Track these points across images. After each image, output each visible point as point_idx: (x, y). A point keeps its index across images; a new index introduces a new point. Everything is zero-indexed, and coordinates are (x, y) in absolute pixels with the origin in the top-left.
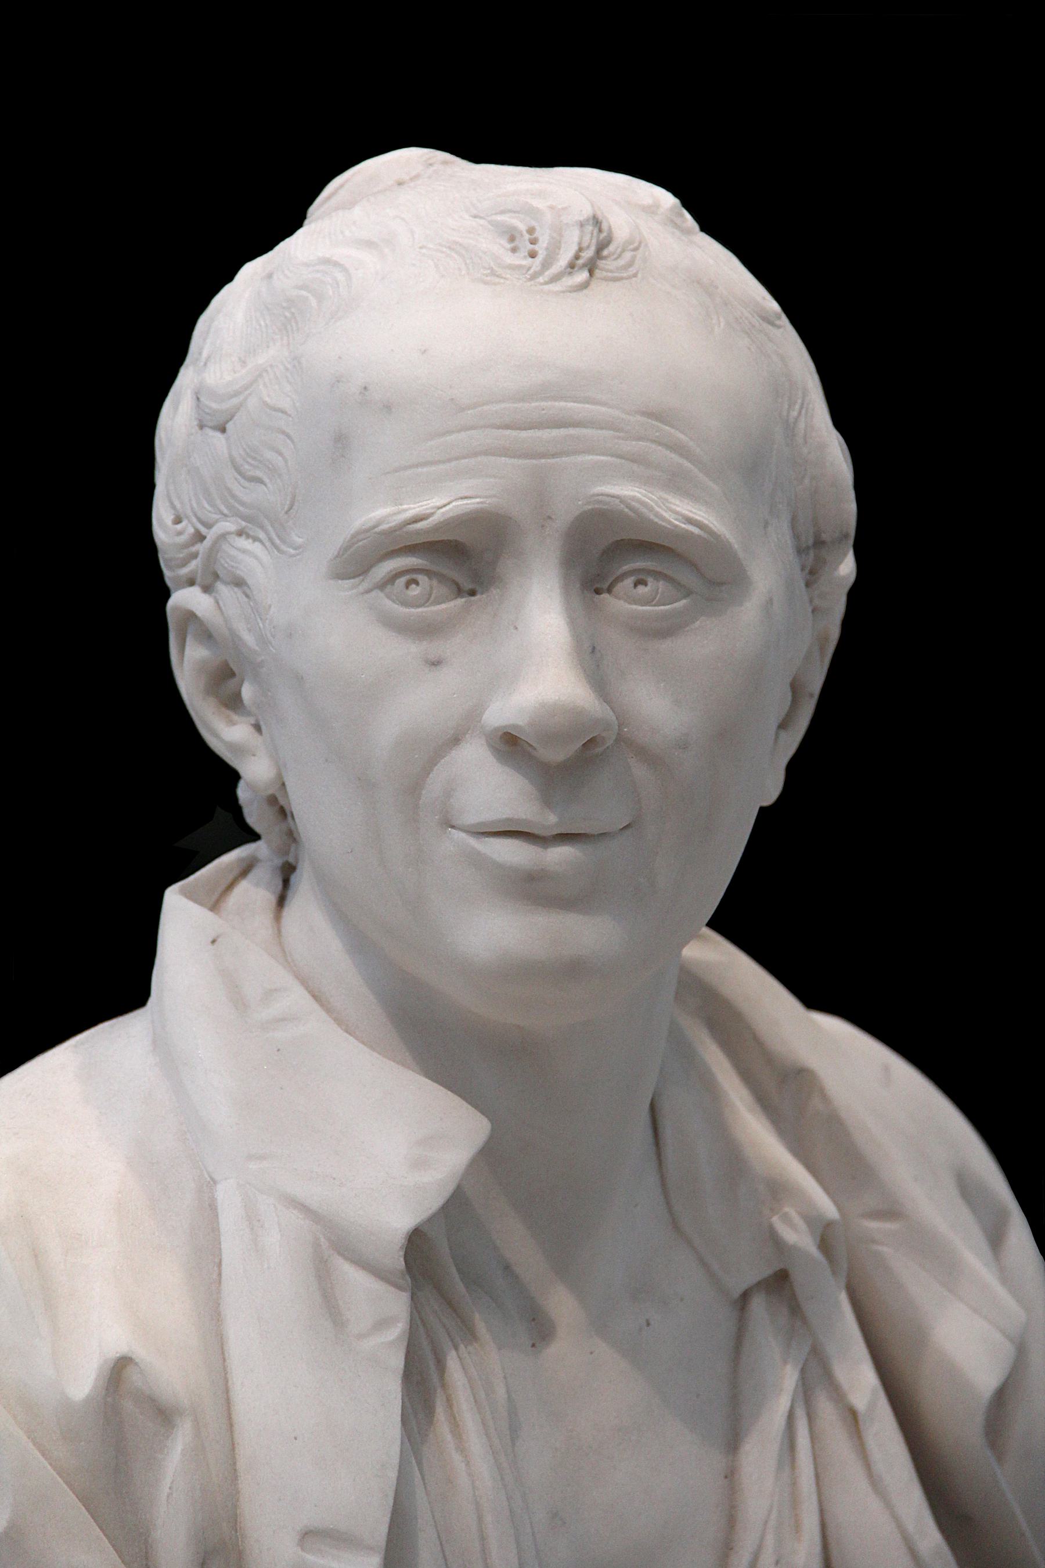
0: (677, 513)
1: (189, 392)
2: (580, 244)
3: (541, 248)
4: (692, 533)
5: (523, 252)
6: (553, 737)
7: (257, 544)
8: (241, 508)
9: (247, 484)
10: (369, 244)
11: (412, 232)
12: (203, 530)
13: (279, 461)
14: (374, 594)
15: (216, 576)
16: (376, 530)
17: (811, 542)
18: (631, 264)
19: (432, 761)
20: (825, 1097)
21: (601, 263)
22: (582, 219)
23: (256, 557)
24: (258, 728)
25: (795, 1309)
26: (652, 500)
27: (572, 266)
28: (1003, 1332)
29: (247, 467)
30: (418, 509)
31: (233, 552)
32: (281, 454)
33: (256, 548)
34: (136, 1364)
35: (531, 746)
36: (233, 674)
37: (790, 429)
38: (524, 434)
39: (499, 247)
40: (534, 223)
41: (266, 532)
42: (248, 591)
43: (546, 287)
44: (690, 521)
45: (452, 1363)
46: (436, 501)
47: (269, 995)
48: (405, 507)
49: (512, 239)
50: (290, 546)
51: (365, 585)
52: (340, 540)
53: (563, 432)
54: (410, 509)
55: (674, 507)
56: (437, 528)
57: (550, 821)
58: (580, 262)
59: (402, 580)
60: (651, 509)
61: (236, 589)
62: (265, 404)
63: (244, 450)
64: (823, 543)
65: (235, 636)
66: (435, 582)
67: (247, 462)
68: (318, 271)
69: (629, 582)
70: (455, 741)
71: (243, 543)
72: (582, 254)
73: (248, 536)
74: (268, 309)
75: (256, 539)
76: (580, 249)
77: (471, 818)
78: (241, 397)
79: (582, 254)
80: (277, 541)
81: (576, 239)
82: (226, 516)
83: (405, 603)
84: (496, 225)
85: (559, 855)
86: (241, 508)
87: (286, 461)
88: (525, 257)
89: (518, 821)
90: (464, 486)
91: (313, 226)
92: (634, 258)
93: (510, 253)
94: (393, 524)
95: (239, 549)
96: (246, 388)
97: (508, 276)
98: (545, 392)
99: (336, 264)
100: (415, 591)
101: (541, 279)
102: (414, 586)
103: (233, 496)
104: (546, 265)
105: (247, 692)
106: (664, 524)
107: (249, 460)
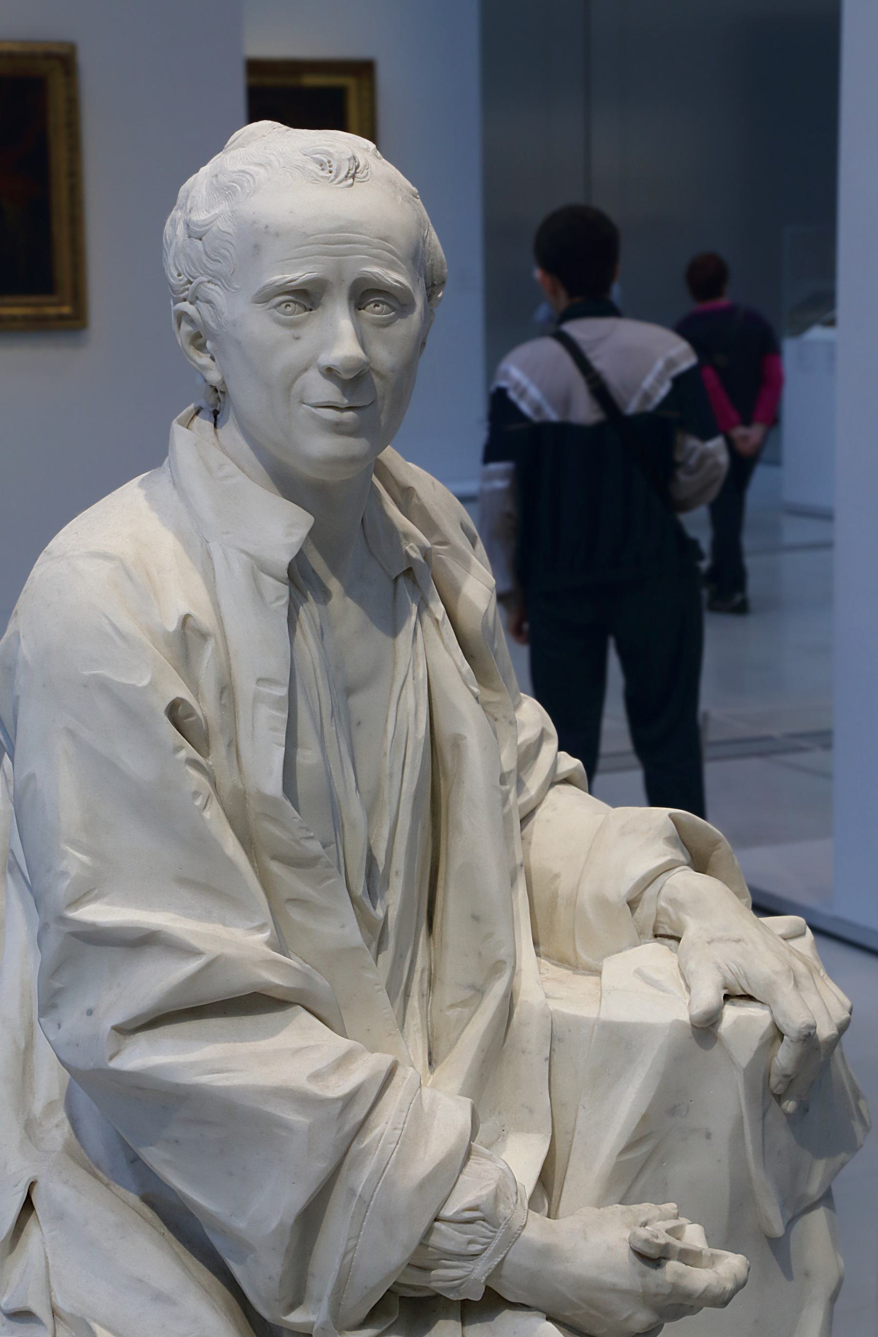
0: (392, 278)
1: (182, 223)
2: (349, 168)
3: (334, 169)
4: (398, 286)
7: (217, 286)
8: (210, 272)
9: (213, 262)
10: (260, 165)
11: (279, 161)
12: (191, 279)
13: (227, 253)
14: (272, 310)
15: (197, 298)
16: (274, 285)
18: (367, 175)
20: (419, 499)
22: (349, 157)
23: (217, 292)
24: (213, 359)
25: (415, 582)
26: (383, 273)
28: (489, 589)
29: (212, 255)
30: (292, 277)
31: (206, 289)
32: (228, 251)
33: (217, 288)
34: (192, 617)
35: (338, 372)
36: (201, 337)
38: (333, 247)
39: (315, 168)
40: (330, 159)
41: (222, 282)
42: (213, 306)
43: (337, 186)
44: (397, 281)
45: (301, 609)
46: (299, 274)
47: (221, 466)
48: (286, 276)
49: (321, 165)
50: (233, 288)
51: (268, 306)
52: (257, 289)
53: (348, 246)
54: (288, 277)
55: (391, 276)
56: (300, 284)
58: (350, 175)
59: (284, 305)
60: (383, 277)
61: (207, 304)
62: (221, 230)
63: (212, 248)
64: (435, 285)
65: (205, 323)
66: (297, 306)
67: (213, 254)
68: (239, 176)
69: (372, 305)
71: (210, 286)
72: (350, 172)
73: (212, 283)
74: (218, 190)
75: (216, 284)
76: (349, 170)
78: (209, 227)
79: (350, 172)
80: (227, 286)
81: (348, 166)
82: (203, 274)
83: (284, 314)
84: (314, 159)
85: (349, 415)
86: (210, 272)
87: (231, 255)
88: (328, 173)
90: (310, 268)
91: (233, 153)
92: (368, 172)
93: (321, 171)
94: (281, 283)
95: (209, 289)
96: (211, 223)
97: (322, 181)
98: (341, 229)
99: (247, 173)
100: (289, 309)
101: (335, 182)
102: (288, 307)
103: (207, 268)
105: (209, 344)
106: (388, 283)
107: (213, 252)
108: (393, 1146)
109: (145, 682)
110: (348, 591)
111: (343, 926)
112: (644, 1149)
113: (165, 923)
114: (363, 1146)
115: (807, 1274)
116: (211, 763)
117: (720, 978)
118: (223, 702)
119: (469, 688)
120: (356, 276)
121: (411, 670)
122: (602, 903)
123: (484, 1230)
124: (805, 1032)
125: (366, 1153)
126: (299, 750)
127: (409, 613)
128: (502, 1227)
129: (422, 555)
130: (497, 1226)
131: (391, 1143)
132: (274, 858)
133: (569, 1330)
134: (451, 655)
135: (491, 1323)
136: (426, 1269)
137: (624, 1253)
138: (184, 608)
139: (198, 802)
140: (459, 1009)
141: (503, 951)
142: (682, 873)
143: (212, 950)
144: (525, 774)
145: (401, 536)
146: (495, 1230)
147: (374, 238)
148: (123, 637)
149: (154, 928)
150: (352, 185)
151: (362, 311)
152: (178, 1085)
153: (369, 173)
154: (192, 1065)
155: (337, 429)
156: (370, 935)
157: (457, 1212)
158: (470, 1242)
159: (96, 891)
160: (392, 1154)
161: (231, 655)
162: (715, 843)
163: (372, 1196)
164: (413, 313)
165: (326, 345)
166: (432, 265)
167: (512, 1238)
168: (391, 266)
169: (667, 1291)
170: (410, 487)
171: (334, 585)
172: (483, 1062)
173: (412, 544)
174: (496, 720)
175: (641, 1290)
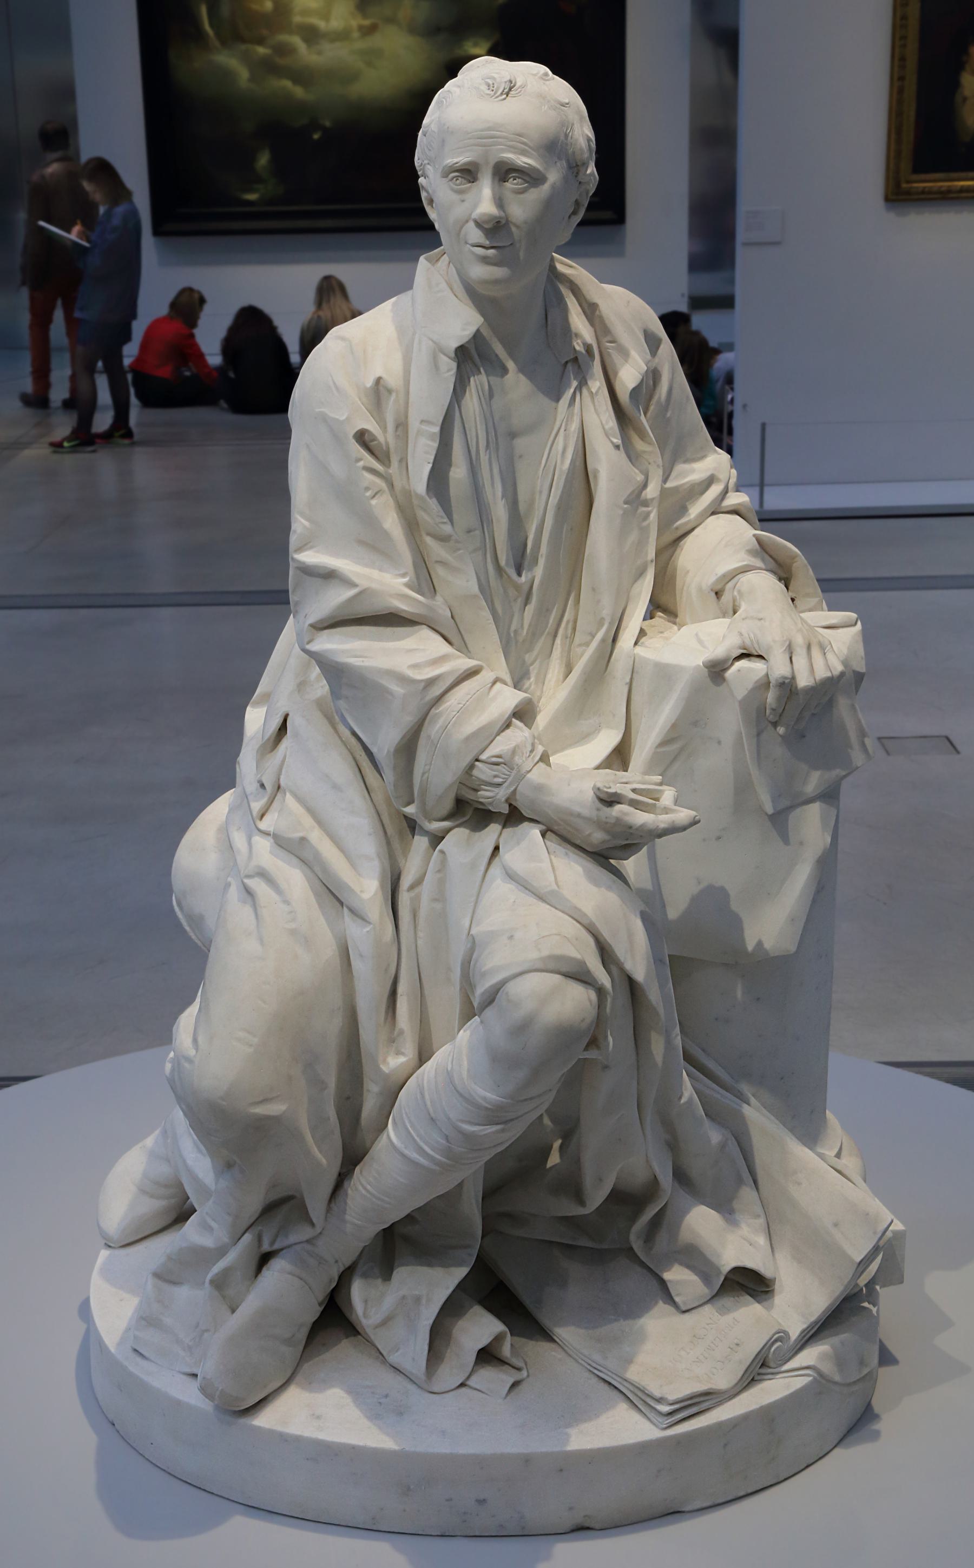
0: (522, 161)
5: (490, 90)
6: (487, 222)
17: (574, 165)
19: (461, 228)
20: (600, 312)
21: (511, 92)
27: (502, 94)
28: (639, 373)
37: (566, 136)
38: (484, 140)
43: (496, 100)
45: (472, 379)
53: (493, 140)
56: (462, 165)
57: (487, 243)
58: (504, 93)
59: (455, 179)
66: (463, 180)
69: (512, 179)
70: (467, 221)
76: (504, 89)
77: (471, 242)
83: (456, 185)
84: (485, 82)
85: (492, 251)
89: (480, 243)
98: (489, 129)
100: (458, 182)
104: (495, 94)
108: (455, 713)
109: (344, 418)
110: (522, 369)
111: (468, 581)
112: (675, 747)
113: (340, 566)
114: (438, 711)
115: (801, 843)
116: (391, 472)
117: (740, 642)
118: (398, 433)
119: (610, 439)
120: (496, 160)
121: (564, 424)
122: (700, 590)
123: (504, 770)
124: (781, 681)
125: (438, 716)
126: (452, 469)
127: (569, 386)
128: (515, 769)
129: (584, 349)
130: (512, 769)
131: (453, 711)
132: (428, 534)
133: (561, 838)
134: (599, 417)
135: (516, 828)
136: (476, 790)
137: (590, 795)
138: (378, 371)
139: (368, 494)
140: (584, 648)
141: (604, 612)
142: (755, 574)
143: (363, 584)
144: (690, 504)
145: (573, 336)
146: (511, 771)
147: (510, 134)
148: (337, 388)
149: (333, 568)
150: (505, 99)
151: (506, 183)
152: (337, 662)
153: (522, 91)
154: (343, 651)
155: (485, 260)
156: (516, 593)
157: (488, 758)
158: (495, 776)
159: (311, 544)
160: (453, 718)
161: (410, 404)
162: (793, 557)
163: (438, 741)
164: (543, 184)
165: (475, 206)
166: (574, 153)
167: (521, 777)
168: (524, 153)
169: (613, 821)
170: (594, 304)
171: (511, 365)
172: (586, 681)
173: (578, 341)
174: (649, 464)
175: (596, 819)
